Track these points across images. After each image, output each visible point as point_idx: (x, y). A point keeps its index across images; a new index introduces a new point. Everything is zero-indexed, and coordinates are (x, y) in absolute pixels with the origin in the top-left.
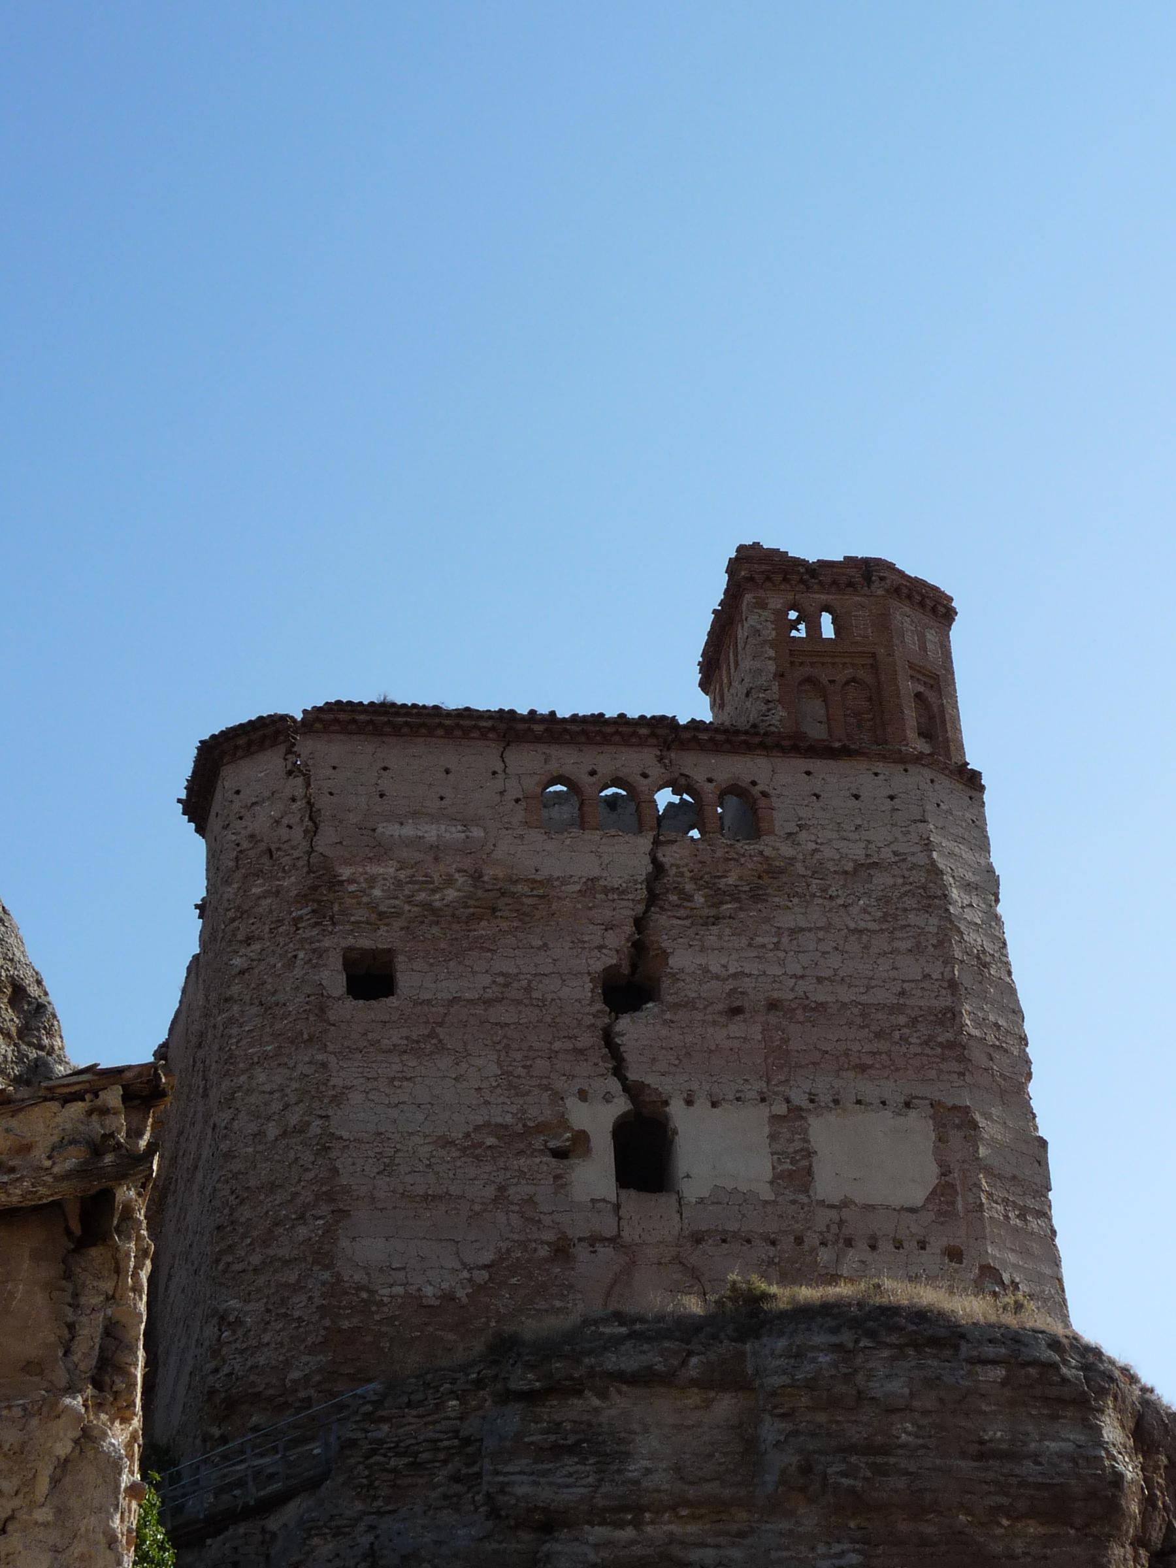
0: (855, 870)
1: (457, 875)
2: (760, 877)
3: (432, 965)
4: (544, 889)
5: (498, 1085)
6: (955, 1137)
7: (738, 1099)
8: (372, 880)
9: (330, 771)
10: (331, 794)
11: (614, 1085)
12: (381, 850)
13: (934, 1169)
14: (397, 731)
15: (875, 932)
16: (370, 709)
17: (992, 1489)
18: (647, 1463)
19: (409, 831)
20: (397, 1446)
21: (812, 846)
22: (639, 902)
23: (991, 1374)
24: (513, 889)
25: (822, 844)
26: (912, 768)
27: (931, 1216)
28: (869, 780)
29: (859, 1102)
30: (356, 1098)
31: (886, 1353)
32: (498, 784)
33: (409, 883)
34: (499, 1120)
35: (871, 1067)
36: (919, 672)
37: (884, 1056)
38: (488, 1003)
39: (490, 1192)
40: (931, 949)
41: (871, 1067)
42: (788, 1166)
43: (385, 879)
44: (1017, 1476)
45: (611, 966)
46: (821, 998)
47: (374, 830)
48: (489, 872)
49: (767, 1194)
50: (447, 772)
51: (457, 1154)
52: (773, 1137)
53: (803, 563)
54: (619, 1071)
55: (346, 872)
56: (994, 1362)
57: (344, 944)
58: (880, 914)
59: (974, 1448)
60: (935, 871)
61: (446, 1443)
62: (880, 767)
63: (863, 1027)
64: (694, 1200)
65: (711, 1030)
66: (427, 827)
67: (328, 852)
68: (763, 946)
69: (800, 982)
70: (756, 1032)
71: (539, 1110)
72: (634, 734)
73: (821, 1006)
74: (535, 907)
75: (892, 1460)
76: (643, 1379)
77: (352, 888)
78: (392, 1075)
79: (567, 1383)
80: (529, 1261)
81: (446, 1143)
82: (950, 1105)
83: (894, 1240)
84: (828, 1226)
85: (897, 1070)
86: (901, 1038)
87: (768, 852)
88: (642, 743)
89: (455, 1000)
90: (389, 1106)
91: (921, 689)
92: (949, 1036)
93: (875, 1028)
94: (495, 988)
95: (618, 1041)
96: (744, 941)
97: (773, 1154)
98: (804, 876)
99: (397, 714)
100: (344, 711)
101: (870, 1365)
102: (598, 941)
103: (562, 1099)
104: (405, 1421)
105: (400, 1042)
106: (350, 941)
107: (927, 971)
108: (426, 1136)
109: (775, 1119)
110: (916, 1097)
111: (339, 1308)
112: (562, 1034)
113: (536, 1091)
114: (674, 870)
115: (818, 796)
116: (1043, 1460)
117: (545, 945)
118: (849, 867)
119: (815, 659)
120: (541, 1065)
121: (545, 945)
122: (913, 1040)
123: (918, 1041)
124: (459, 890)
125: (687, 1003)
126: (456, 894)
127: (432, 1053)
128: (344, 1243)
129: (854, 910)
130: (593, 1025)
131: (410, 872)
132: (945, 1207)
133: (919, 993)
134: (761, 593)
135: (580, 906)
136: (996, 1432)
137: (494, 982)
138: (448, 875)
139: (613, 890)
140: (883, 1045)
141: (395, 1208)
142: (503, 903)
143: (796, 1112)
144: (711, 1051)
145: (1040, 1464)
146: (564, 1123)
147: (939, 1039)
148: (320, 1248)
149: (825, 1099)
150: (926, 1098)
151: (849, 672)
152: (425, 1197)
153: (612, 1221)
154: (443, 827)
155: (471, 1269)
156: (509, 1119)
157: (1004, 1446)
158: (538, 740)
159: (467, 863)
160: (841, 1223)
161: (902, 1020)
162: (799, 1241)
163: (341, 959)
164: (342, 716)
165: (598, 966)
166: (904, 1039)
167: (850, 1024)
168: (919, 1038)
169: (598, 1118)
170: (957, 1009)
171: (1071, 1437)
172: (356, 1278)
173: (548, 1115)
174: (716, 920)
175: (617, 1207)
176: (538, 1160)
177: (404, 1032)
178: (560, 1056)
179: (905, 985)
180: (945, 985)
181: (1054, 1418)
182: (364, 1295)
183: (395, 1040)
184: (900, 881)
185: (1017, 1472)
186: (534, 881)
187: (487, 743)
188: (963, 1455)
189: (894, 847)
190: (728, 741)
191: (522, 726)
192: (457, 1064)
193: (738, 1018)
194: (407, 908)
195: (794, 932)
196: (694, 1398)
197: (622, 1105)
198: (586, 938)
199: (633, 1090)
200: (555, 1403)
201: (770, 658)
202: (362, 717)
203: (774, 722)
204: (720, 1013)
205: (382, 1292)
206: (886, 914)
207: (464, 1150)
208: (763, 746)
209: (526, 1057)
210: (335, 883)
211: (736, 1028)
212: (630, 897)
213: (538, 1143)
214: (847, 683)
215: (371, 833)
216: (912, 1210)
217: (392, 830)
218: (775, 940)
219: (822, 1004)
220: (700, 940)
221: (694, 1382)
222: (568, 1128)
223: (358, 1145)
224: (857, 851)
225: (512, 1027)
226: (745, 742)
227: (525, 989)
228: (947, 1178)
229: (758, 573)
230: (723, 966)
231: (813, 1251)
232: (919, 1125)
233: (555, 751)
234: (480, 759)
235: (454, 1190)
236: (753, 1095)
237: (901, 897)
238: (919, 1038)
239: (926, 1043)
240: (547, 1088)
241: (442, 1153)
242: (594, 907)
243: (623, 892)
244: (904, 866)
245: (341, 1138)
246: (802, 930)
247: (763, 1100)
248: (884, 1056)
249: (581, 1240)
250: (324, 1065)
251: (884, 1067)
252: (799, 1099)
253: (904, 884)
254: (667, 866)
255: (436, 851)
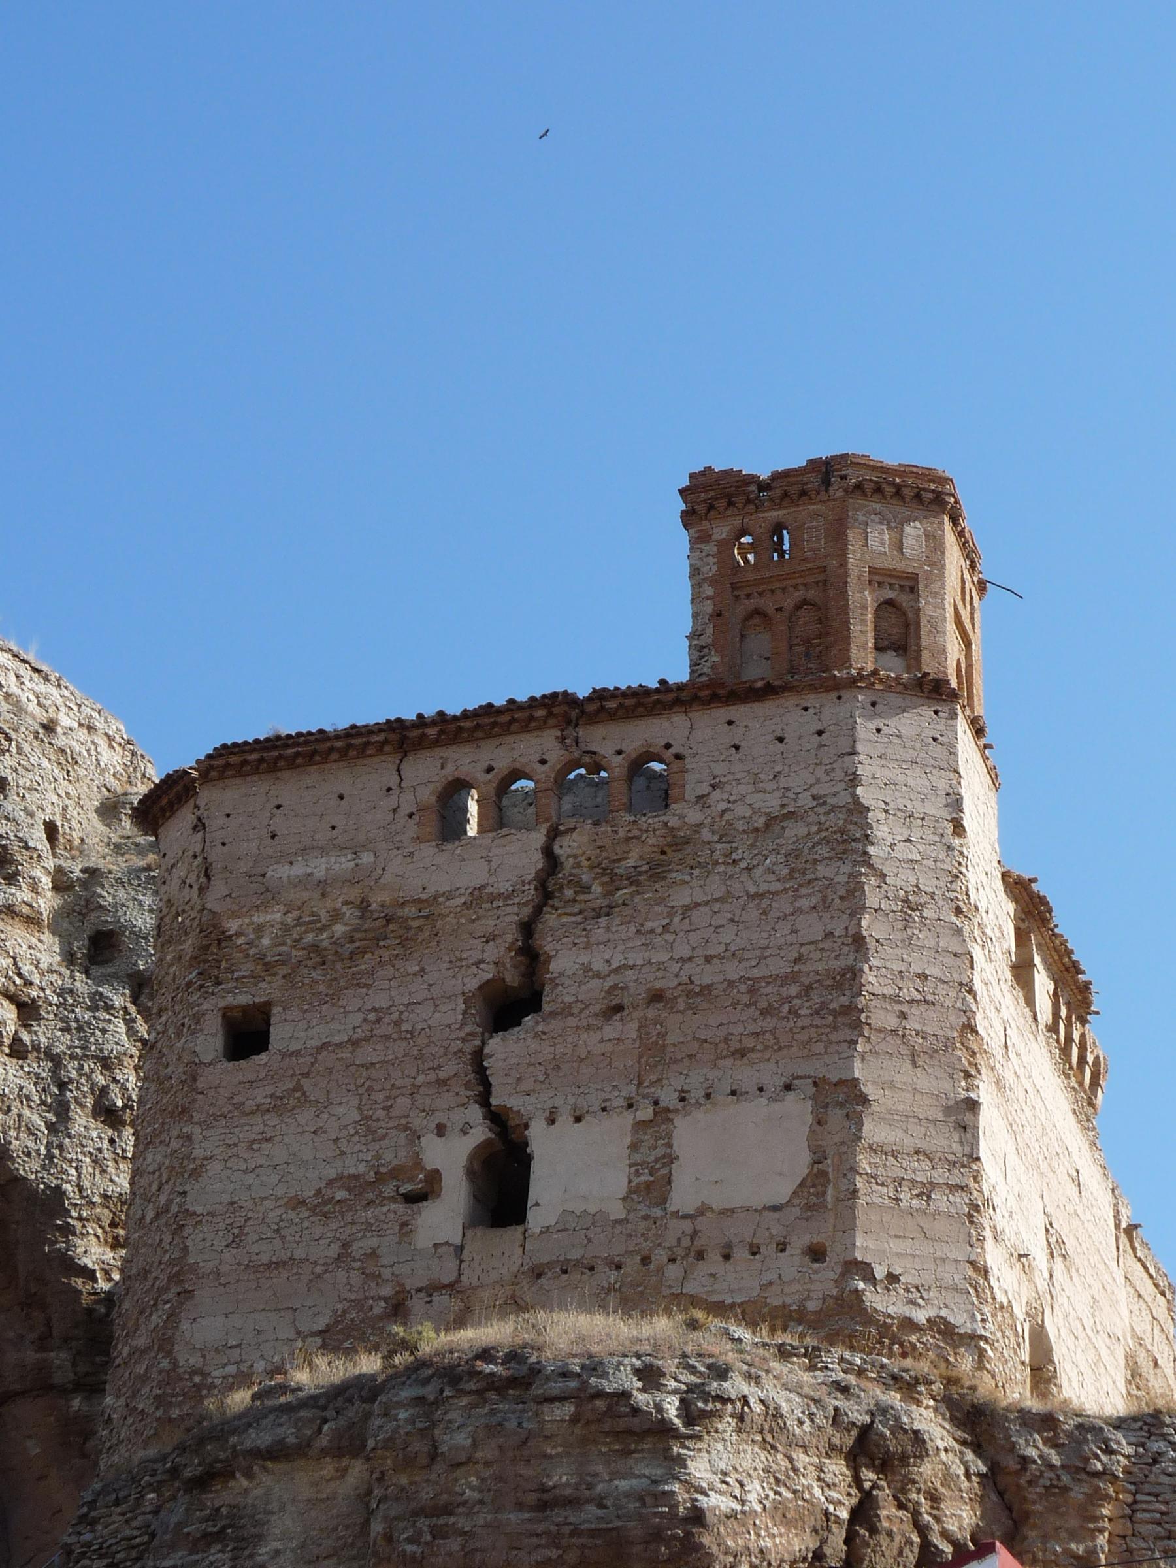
0: (767, 825)
1: (345, 909)
2: (663, 852)
3: (305, 1011)
4: (428, 907)
5: (357, 1132)
6: (836, 1116)
7: (604, 1109)
8: (260, 929)
9: (222, 821)
10: (224, 844)
11: (475, 1113)
12: (268, 895)
13: (806, 1157)
14: (291, 764)
15: (777, 893)
16: (257, 746)
17: (543, 1541)
18: (277, 1545)
19: (298, 870)
20: (101, 1548)
21: (723, 806)
22: (525, 904)
23: (557, 1412)
24: (400, 913)
25: (735, 801)
26: (846, 694)
27: (796, 1211)
28: (789, 716)
29: (733, 1093)
30: (215, 1167)
31: (464, 1401)
32: (392, 801)
33: (296, 926)
34: (352, 1171)
35: (753, 1050)
36: (890, 576)
37: (768, 1036)
38: (355, 1043)
39: (335, 1249)
40: (837, 901)
41: (753, 1050)
42: (646, 1178)
43: (273, 926)
44: (570, 1524)
45: (488, 981)
46: (706, 980)
47: (263, 875)
48: (376, 900)
49: (617, 1211)
50: (341, 797)
51: (307, 1214)
52: (634, 1147)
53: (752, 479)
54: (484, 1099)
55: (232, 926)
56: (562, 1399)
57: (222, 1004)
58: (786, 871)
59: (532, 1498)
60: (860, 810)
61: (138, 1540)
62: (811, 700)
63: (748, 1006)
64: (538, 1230)
65: (584, 1036)
66: (316, 862)
67: (217, 908)
68: (652, 931)
69: (687, 965)
70: (631, 1030)
71: (394, 1154)
72: (532, 718)
73: (706, 990)
74: (420, 929)
75: (452, 1520)
76: (277, 1453)
77: (240, 941)
78: (253, 1137)
79: (218, 1465)
80: (363, 1321)
81: (298, 1203)
82: (834, 1080)
83: (751, 1245)
84: (679, 1240)
85: (780, 1048)
86: (790, 1012)
87: (674, 822)
88: (543, 725)
89: (325, 1046)
90: (245, 1172)
91: (891, 594)
92: (844, 1000)
93: (763, 1004)
94: (366, 1027)
95: (486, 1064)
96: (633, 928)
97: (630, 1166)
98: (709, 843)
99: (286, 746)
100: (232, 753)
101: (449, 1417)
102: (476, 955)
103: (419, 1138)
104: (110, 1520)
105: (263, 1101)
106: (230, 1000)
107: (829, 928)
108: (277, 1199)
109: (640, 1125)
110: (798, 1078)
111: (173, 1396)
112: (427, 1065)
113: (394, 1133)
114: (571, 861)
115: (737, 748)
116: (608, 1503)
117: (423, 970)
118: (760, 822)
119: (762, 588)
120: (403, 1102)
121: (423, 970)
122: (802, 1012)
123: (808, 1012)
124: (346, 925)
125: (563, 1009)
126: (344, 928)
127: (294, 1108)
128: (185, 1325)
129: (758, 872)
130: (460, 1051)
131: (296, 913)
132: (813, 1200)
133: (816, 955)
134: (706, 525)
135: (463, 921)
136: (561, 1477)
137: (365, 1020)
138: (335, 910)
139: (500, 895)
140: (769, 1023)
141: (238, 1281)
142: (391, 929)
143: (663, 1115)
144: (582, 1060)
145: (606, 1507)
146: (418, 1163)
147: (833, 1006)
148: (163, 1334)
149: (697, 1094)
150: (809, 1077)
151: (798, 595)
152: (268, 1266)
153: (452, 1264)
154: (333, 859)
155: (306, 1337)
156: (362, 1168)
157: (568, 1492)
158: (436, 743)
159: (354, 894)
160: (694, 1234)
161: (794, 990)
162: (646, 1261)
163: (220, 1020)
164: (233, 760)
165: (473, 984)
166: (793, 1012)
167: (735, 1005)
168: (810, 1008)
169: (451, 1155)
170: (857, 967)
171: (647, 1472)
172: (192, 1361)
173: (403, 1158)
174: (609, 911)
175: (460, 1249)
176: (385, 1209)
177: (269, 1090)
178: (423, 1090)
179: (803, 950)
180: (849, 940)
181: (626, 1453)
182: (197, 1379)
183: (259, 1100)
184: (815, 828)
185: (572, 1519)
186: (420, 901)
187: (383, 758)
188: (520, 1506)
189: (815, 791)
190: (639, 704)
191: (415, 733)
192: (318, 1116)
193: (617, 1017)
194: (294, 952)
195: (687, 909)
196: (328, 1469)
197: (481, 1133)
198: (464, 956)
199: (497, 1118)
200: (219, 1487)
201: (708, 598)
202: (253, 757)
203: (705, 670)
204: (596, 1015)
205: (214, 1374)
206: (792, 871)
207: (313, 1209)
208: (678, 702)
209: (388, 1098)
210: (223, 939)
211: (611, 1030)
212: (517, 900)
213: (388, 1190)
214: (798, 607)
215: (260, 878)
216: (775, 1208)
217: (281, 872)
218: (665, 922)
219: (708, 986)
220: (586, 936)
221: (324, 1452)
222: (423, 1169)
223: (210, 1219)
224: (772, 803)
225: (378, 1066)
226: (658, 701)
227: (395, 1023)
228: (820, 1166)
229: (713, 499)
230: (607, 961)
231: (660, 1269)
232: (798, 1110)
233: (450, 753)
234: (377, 774)
235: (299, 1253)
236: (621, 1102)
237: (813, 847)
238: (810, 1008)
239: (817, 1012)
240: (406, 1128)
241: (291, 1215)
242: (478, 918)
243: (509, 897)
244: (821, 810)
245: (194, 1213)
246: (697, 905)
247: (630, 1106)
248: (768, 1036)
249: (419, 1290)
250: (189, 1138)
251: (766, 1047)
252: (668, 1098)
253: (820, 831)
254: (562, 859)
255: (323, 887)
